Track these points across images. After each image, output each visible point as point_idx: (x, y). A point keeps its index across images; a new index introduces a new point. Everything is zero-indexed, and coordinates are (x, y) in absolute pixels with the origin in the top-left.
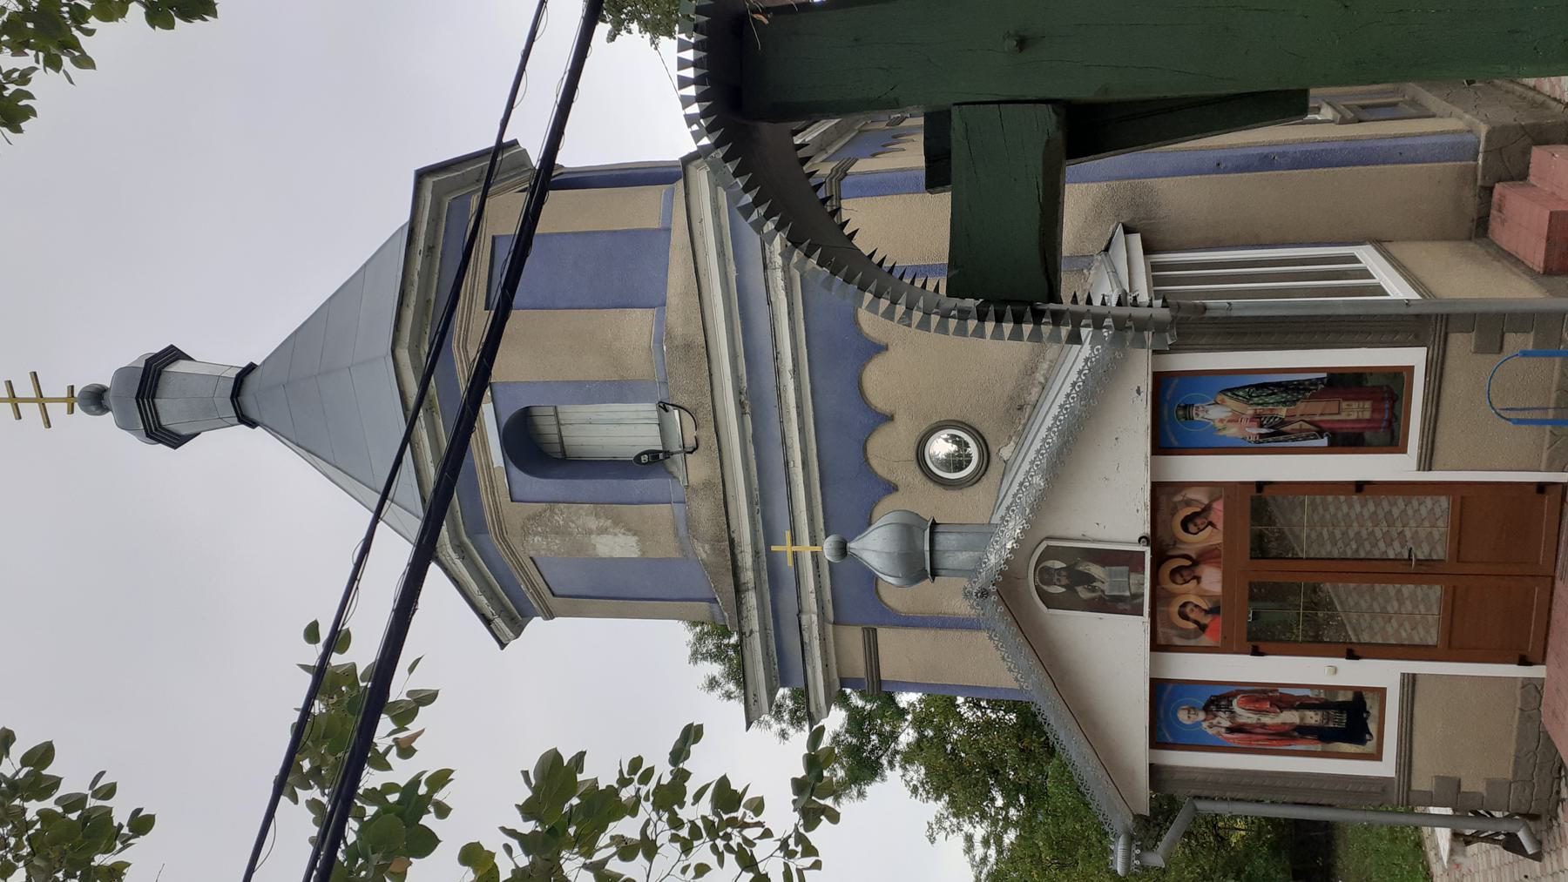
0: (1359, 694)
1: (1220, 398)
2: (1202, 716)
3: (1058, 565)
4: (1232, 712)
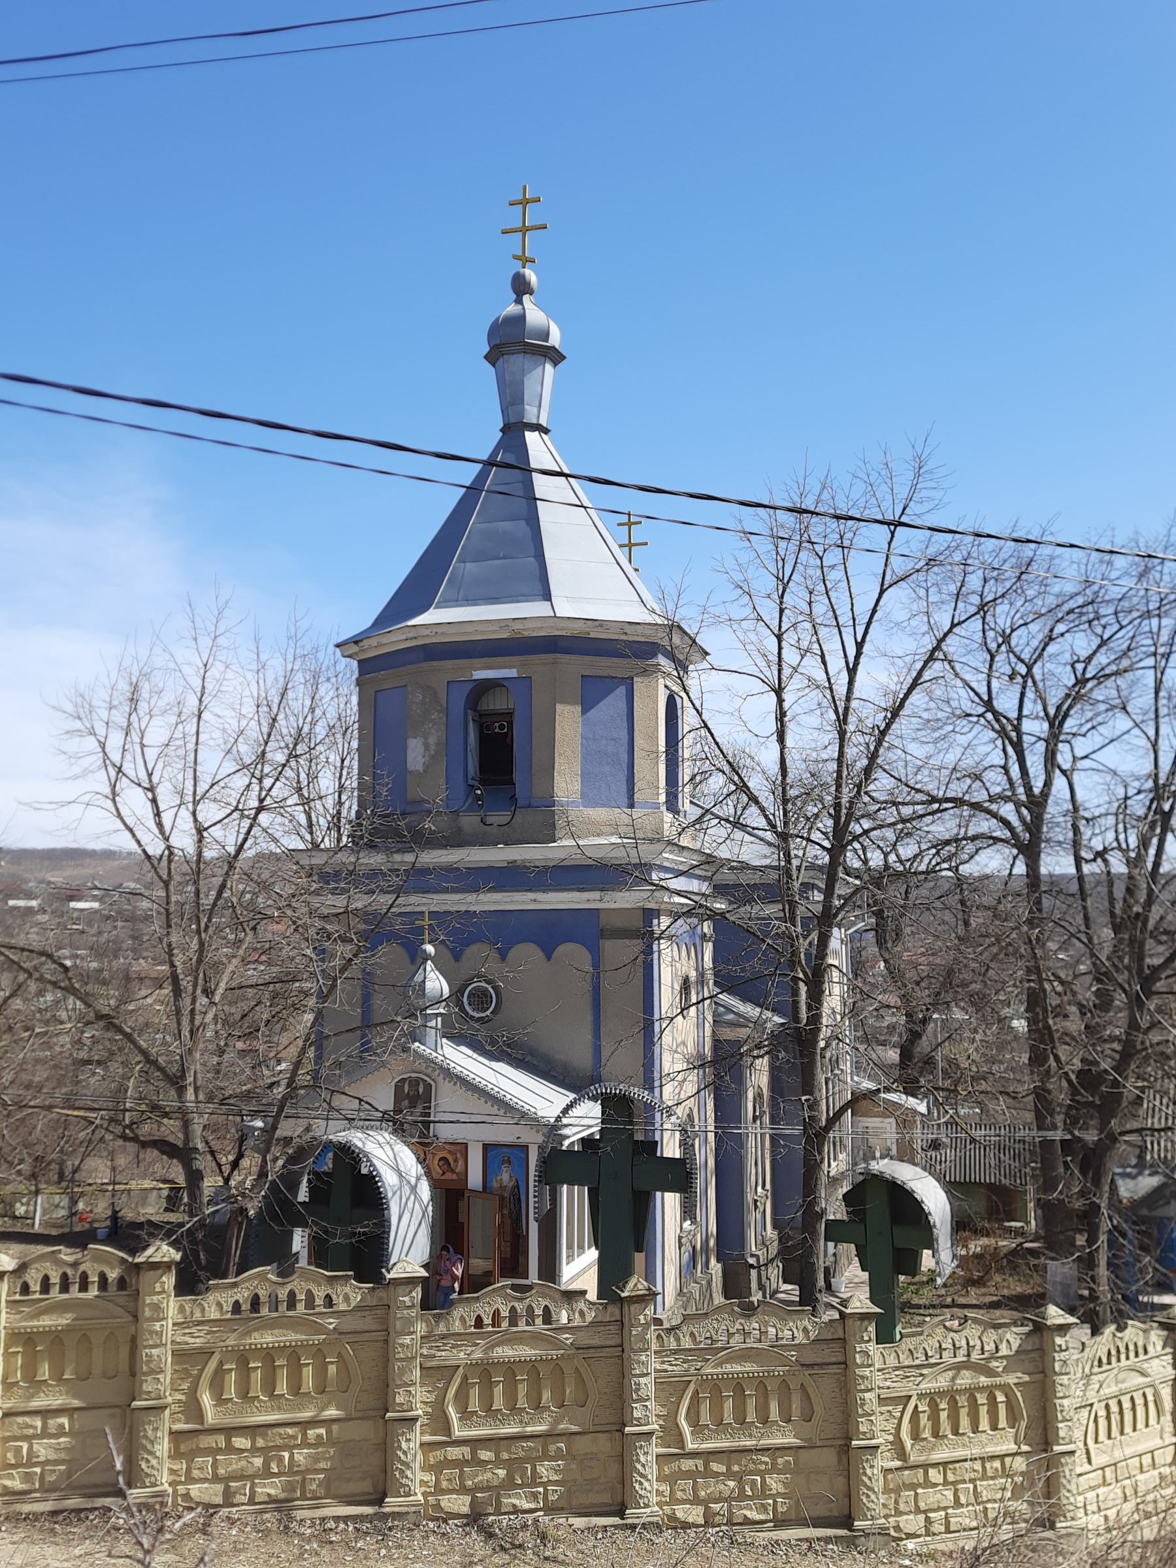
0: (173, 1354)
3: (421, 1090)
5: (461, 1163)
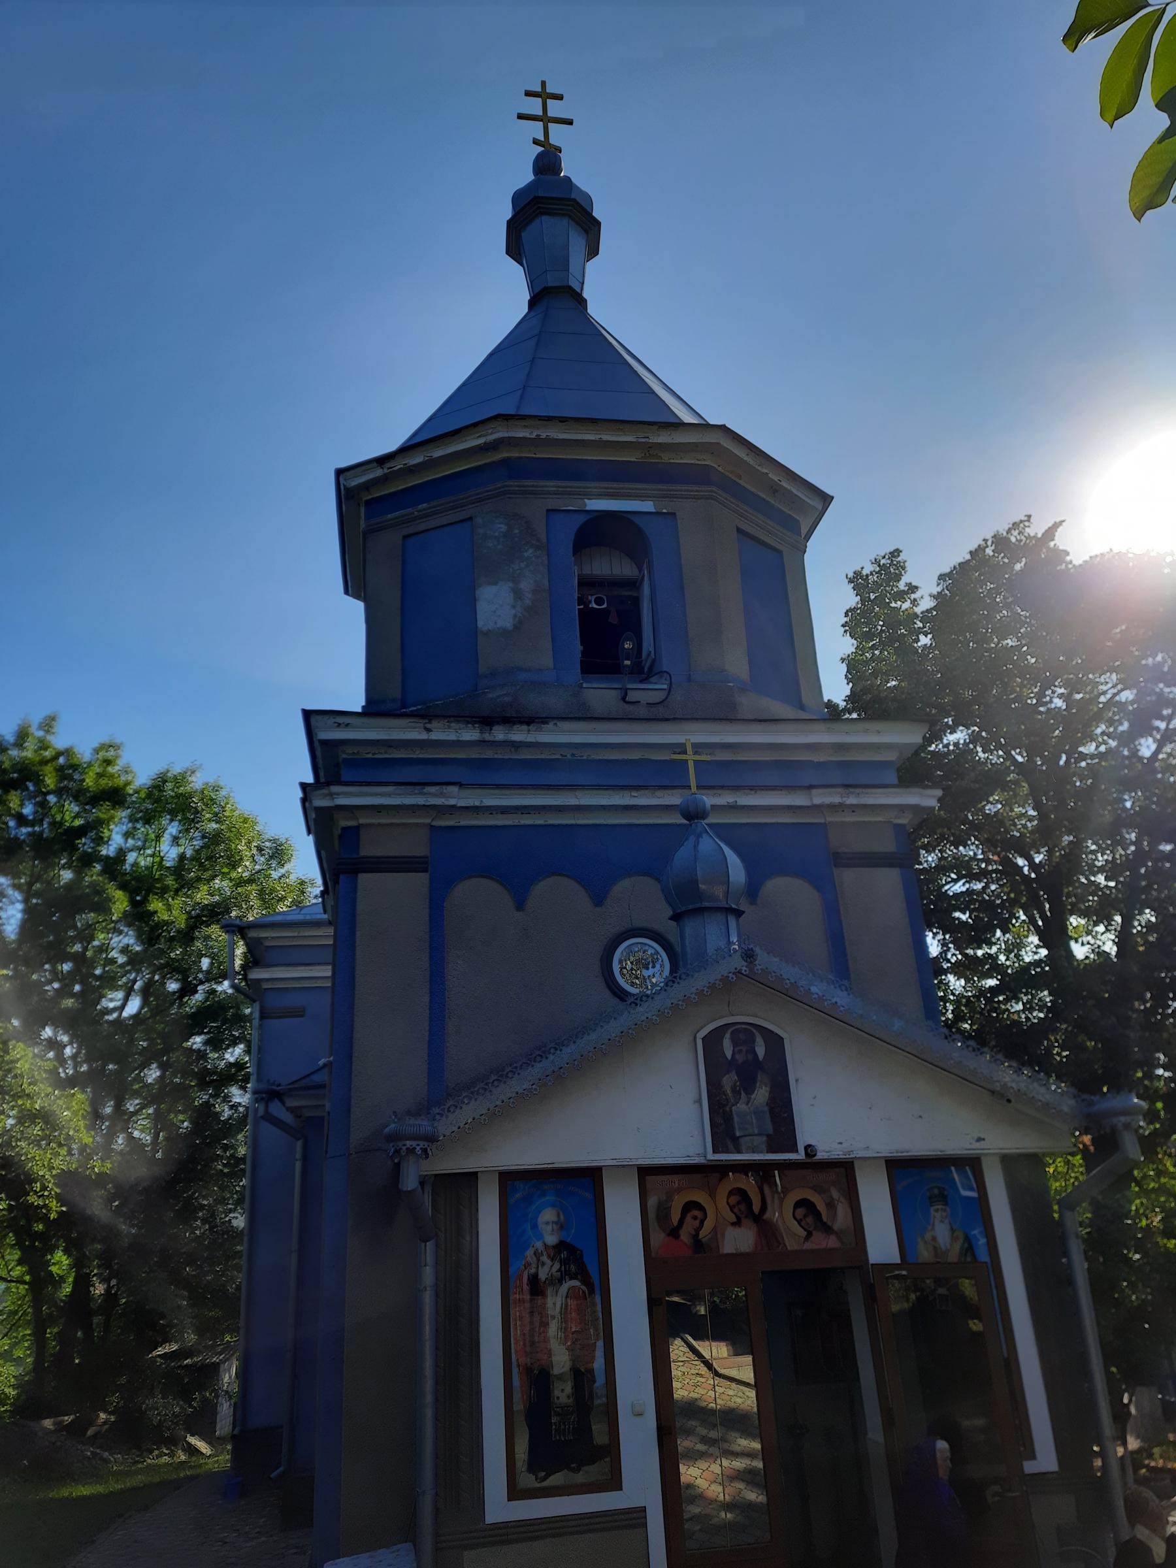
0: (611, 1451)
1: (960, 1234)
2: (552, 1240)
3: (761, 1051)
4: (560, 1281)
5: (842, 1211)
